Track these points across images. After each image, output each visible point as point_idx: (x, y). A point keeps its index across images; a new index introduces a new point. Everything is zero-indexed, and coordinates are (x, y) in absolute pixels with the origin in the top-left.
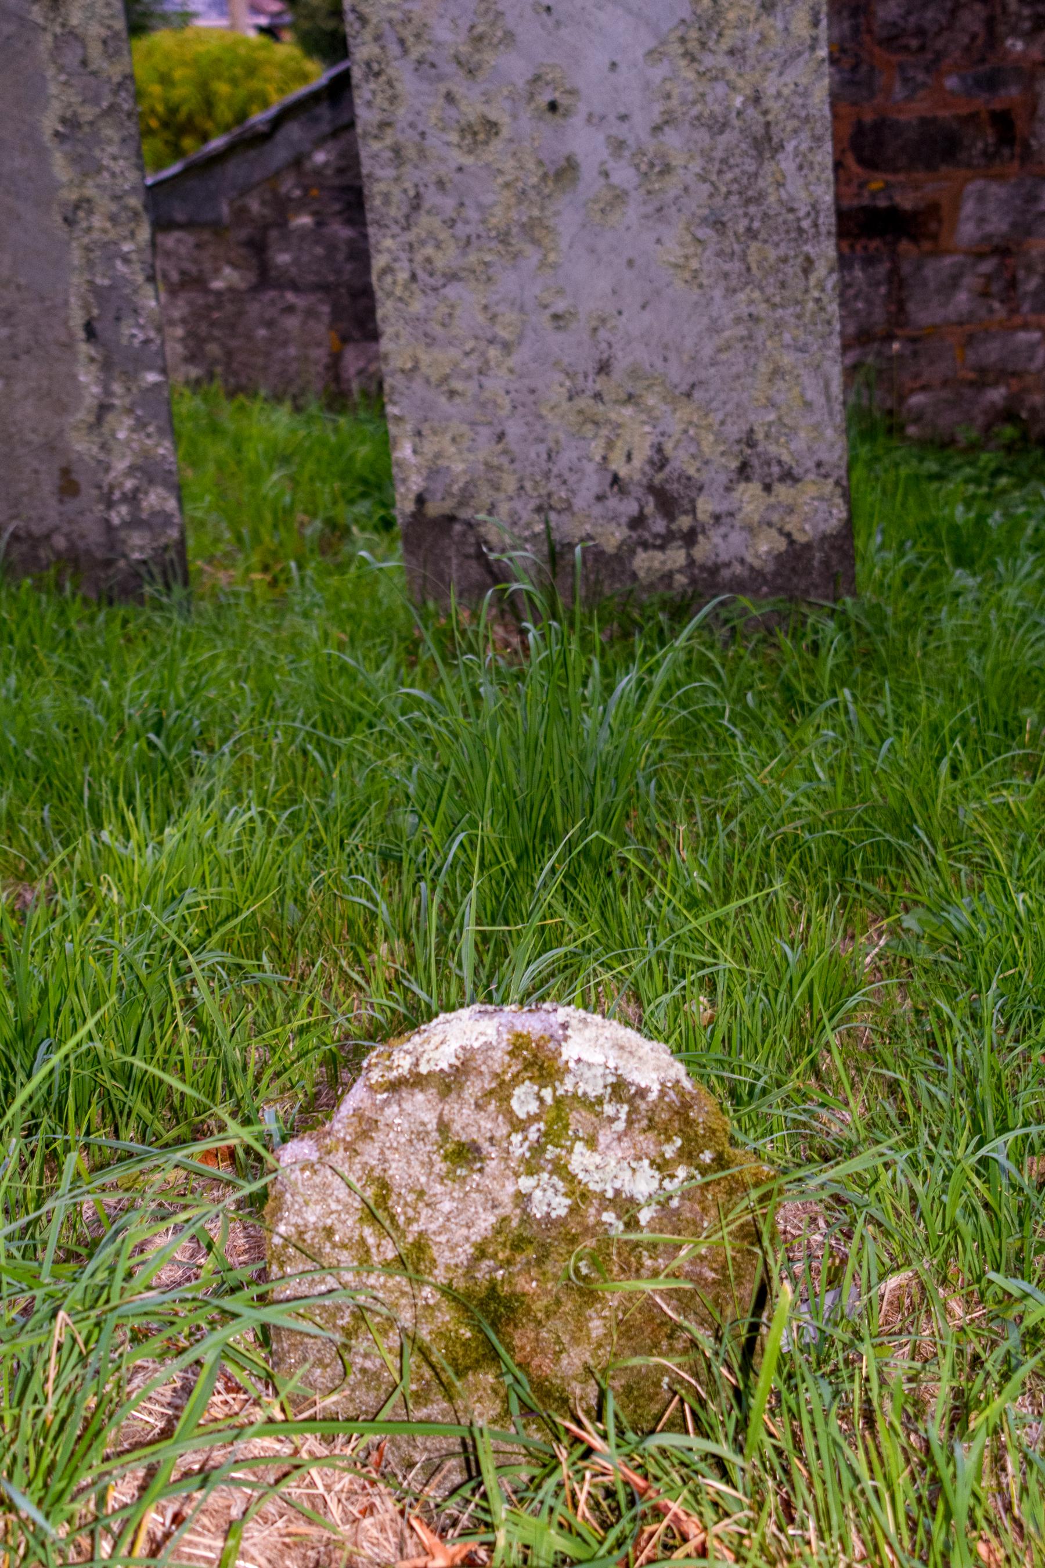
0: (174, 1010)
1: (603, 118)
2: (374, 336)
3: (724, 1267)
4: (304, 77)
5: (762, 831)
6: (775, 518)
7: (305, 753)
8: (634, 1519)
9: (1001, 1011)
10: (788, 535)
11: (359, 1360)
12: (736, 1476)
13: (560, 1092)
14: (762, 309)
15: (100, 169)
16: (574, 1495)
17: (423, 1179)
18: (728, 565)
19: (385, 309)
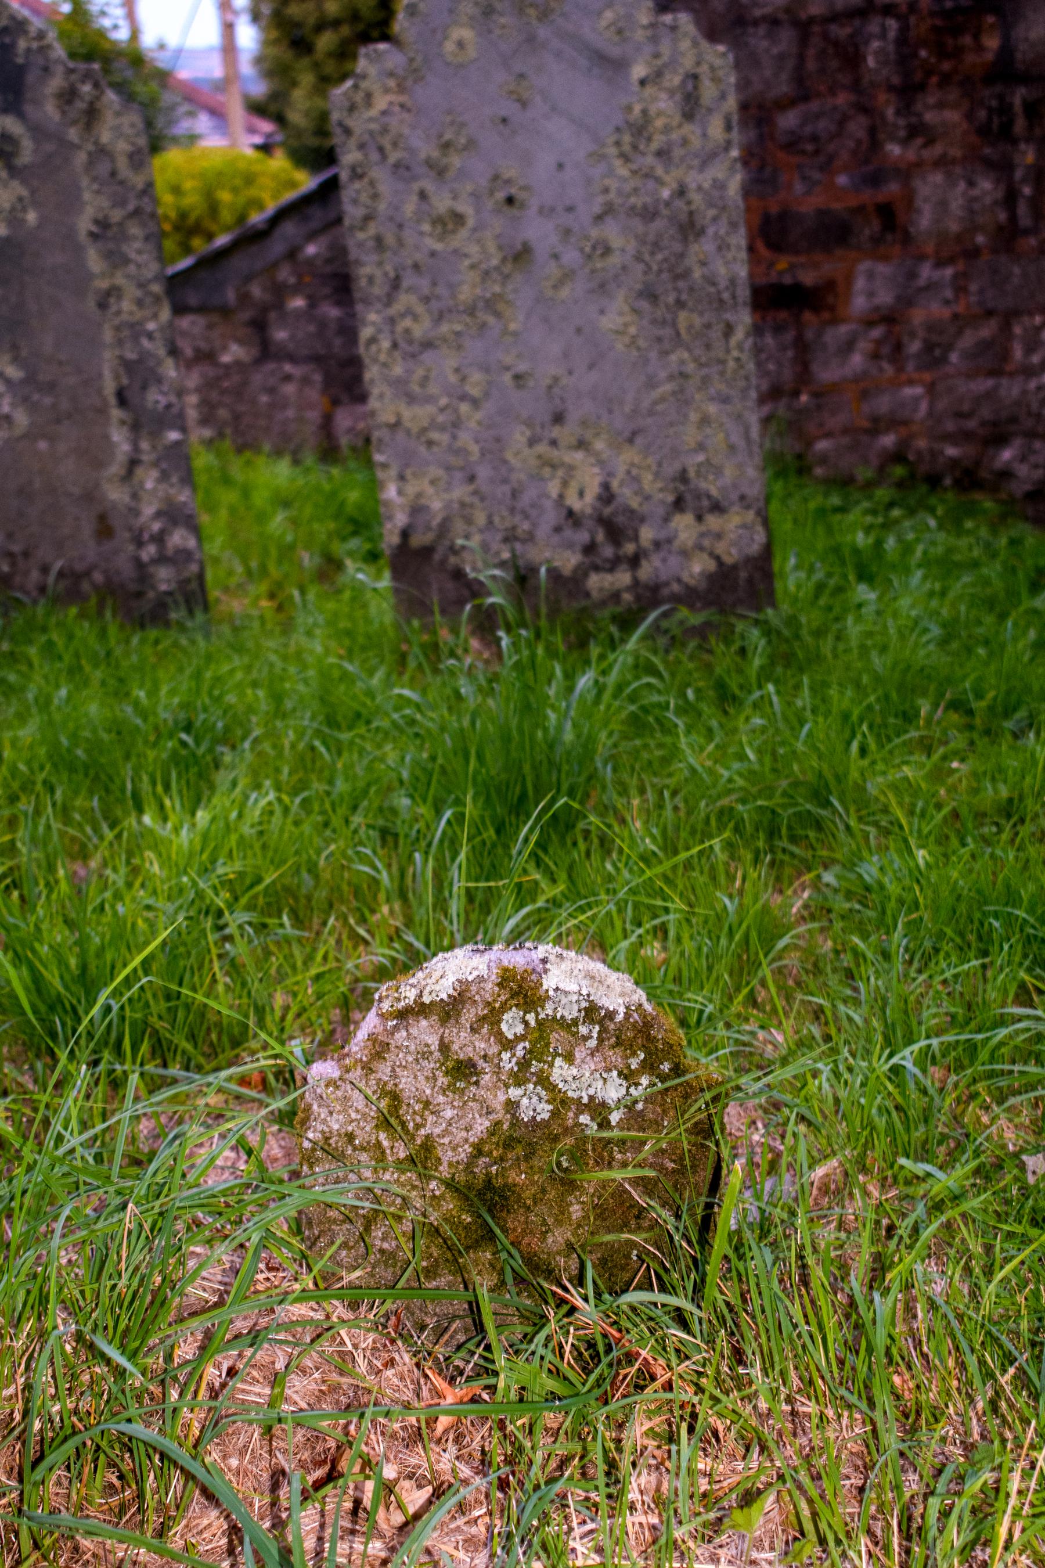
0: (211, 961)
1: (552, 210)
2: (362, 398)
3: (682, 1158)
4: (293, 184)
5: (703, 804)
6: (706, 543)
7: (313, 749)
8: (610, 1365)
9: (907, 949)
10: (718, 558)
11: (378, 1243)
12: (696, 1328)
13: (542, 1016)
14: (690, 367)
15: (126, 261)
16: (561, 1346)
17: (428, 1092)
18: (667, 584)
19: (372, 373)
